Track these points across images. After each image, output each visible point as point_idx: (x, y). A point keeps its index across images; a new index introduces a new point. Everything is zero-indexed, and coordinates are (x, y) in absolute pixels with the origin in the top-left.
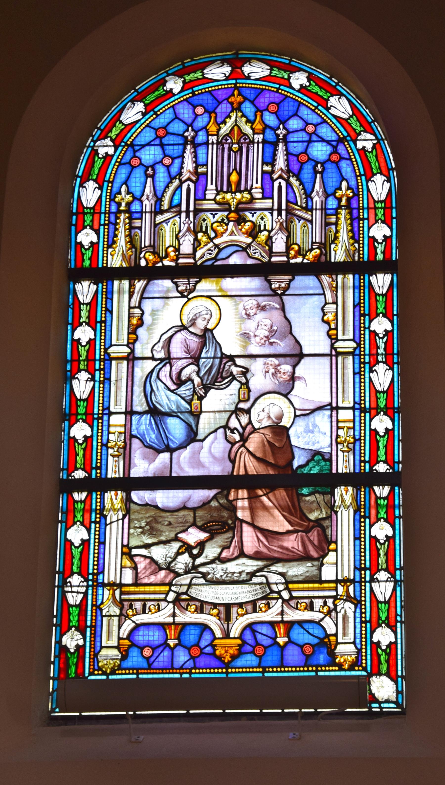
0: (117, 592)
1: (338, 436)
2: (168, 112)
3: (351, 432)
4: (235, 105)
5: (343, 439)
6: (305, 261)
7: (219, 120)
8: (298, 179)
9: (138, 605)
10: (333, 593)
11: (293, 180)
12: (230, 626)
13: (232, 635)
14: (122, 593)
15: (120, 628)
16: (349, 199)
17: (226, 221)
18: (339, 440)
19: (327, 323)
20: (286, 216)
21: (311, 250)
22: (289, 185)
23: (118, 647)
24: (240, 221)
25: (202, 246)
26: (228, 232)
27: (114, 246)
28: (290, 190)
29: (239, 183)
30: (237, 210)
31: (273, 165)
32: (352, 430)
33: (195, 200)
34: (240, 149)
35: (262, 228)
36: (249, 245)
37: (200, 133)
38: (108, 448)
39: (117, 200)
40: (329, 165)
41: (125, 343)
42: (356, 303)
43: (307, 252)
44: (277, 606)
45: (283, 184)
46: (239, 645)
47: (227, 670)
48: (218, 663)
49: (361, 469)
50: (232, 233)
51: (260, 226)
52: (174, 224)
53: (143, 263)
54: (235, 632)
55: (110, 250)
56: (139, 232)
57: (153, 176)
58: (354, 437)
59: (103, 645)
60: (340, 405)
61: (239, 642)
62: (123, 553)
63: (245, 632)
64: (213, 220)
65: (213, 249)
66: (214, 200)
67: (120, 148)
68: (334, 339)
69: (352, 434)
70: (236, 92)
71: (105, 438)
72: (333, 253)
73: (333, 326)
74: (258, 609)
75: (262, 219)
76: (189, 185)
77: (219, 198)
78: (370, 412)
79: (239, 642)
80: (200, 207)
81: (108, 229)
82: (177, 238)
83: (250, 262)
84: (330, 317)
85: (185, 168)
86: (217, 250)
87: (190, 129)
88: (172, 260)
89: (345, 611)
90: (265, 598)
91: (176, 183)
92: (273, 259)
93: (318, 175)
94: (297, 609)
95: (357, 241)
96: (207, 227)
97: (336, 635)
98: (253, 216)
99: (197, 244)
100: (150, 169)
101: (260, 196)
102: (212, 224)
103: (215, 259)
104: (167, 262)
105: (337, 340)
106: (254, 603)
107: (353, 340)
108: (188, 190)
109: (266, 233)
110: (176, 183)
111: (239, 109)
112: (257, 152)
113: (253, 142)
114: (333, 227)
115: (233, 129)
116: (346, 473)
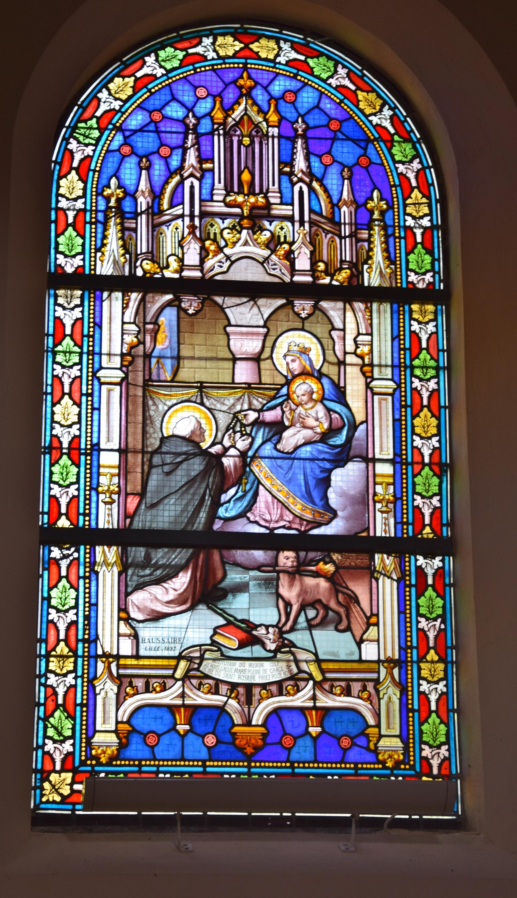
0: (114, 667)
1: (375, 494)
2: (163, 92)
5: (106, 488)
6: (334, 283)
8: (322, 185)
9: (140, 683)
10: (374, 676)
11: (315, 185)
12: (252, 710)
13: (254, 723)
14: (118, 667)
15: (117, 710)
16: (119, 201)
18: (376, 498)
20: (310, 227)
21: (341, 269)
22: (312, 190)
23: (116, 731)
24: (256, 228)
25: (210, 257)
26: (241, 242)
27: (370, 262)
28: (313, 196)
29: (252, 184)
30: (251, 217)
31: (292, 166)
32: (117, 478)
33: (201, 200)
34: (252, 142)
35: (282, 239)
37: (203, 121)
38: (98, 493)
39: (105, 193)
40: (356, 169)
41: (119, 366)
43: (335, 271)
44: (308, 690)
45: (305, 189)
46: (263, 734)
47: (249, 764)
48: (239, 755)
49: (403, 533)
50: (246, 243)
51: (279, 237)
52: (177, 229)
54: (258, 718)
55: (99, 254)
57: (148, 169)
58: (394, 496)
59: (97, 729)
60: (377, 456)
61: (263, 730)
62: (120, 619)
63: (269, 719)
64: (223, 226)
65: (224, 260)
66: (224, 201)
67: (107, 132)
68: (369, 377)
69: (117, 481)
70: (245, 75)
71: (95, 482)
72: (366, 275)
74: (285, 692)
76: (301, 188)
77: (228, 199)
78: (50, 453)
79: (263, 730)
80: (209, 209)
81: (96, 228)
83: (268, 279)
85: (296, 167)
86: (229, 263)
87: (190, 115)
88: (176, 271)
89: (390, 698)
90: (292, 678)
92: (296, 278)
93: (144, 172)
94: (331, 692)
95: (393, 262)
97: (378, 726)
98: (270, 225)
100: (144, 160)
101: (278, 201)
102: (222, 231)
104: (168, 274)
105: (373, 379)
106: (279, 684)
107: (392, 380)
108: (192, 187)
110: (177, 178)
111: (249, 95)
112: (272, 150)
113: (267, 135)
114: (366, 244)
115: (242, 118)
116: (108, 529)
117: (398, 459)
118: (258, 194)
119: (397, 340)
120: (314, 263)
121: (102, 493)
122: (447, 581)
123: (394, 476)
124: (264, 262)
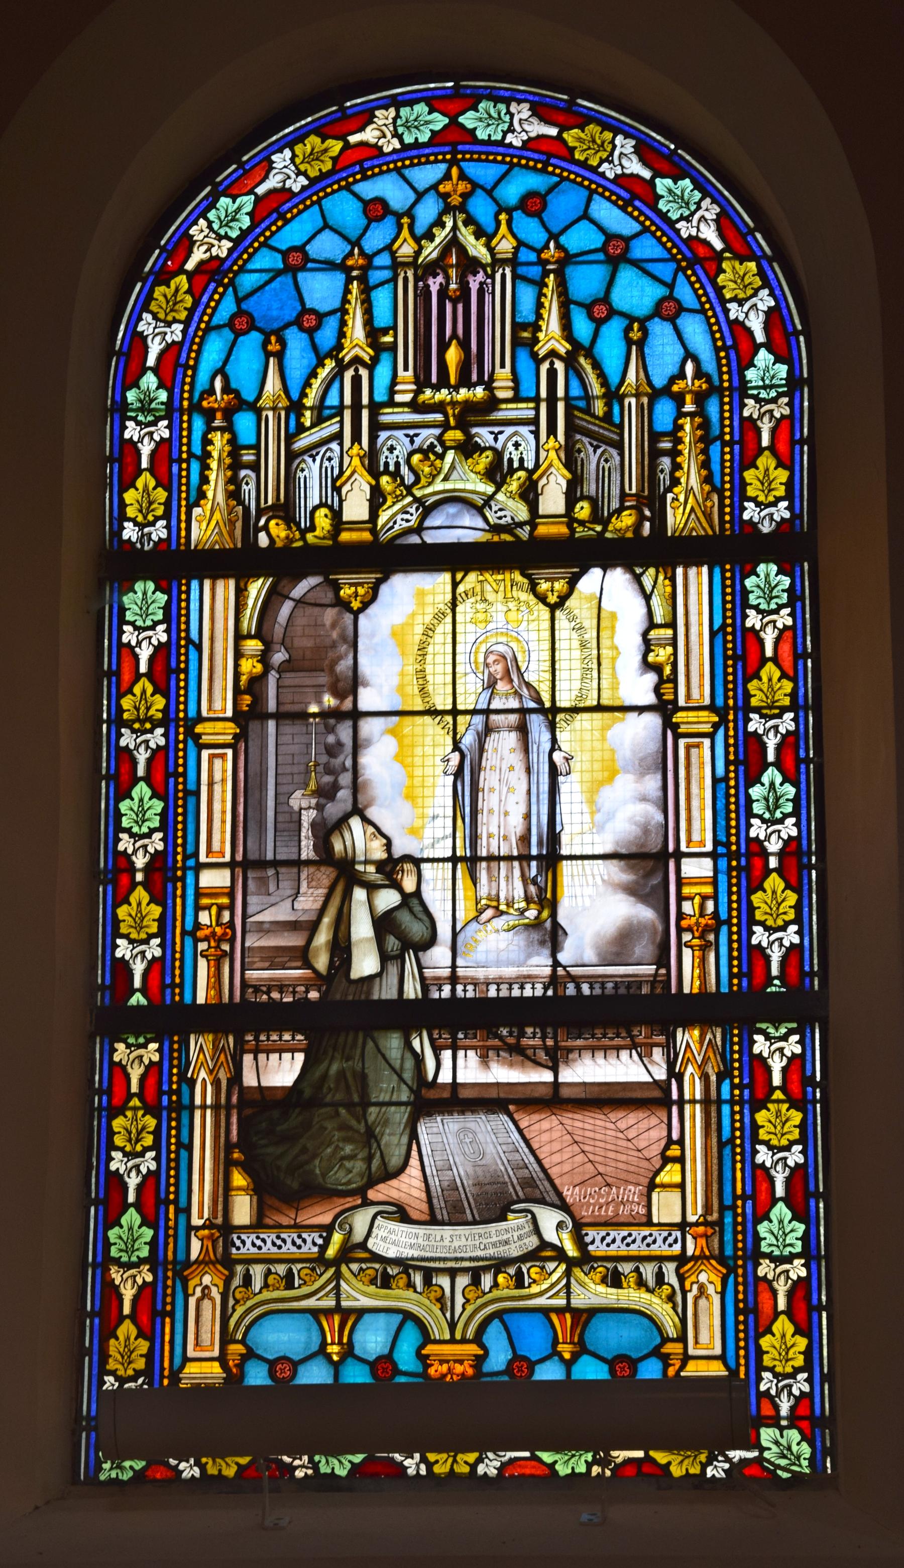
1: (680, 916)
3: (710, 906)
4: (456, 200)
7: (420, 230)
17: (439, 449)
19: (657, 668)
27: (676, 490)
35: (516, 465)
36: (489, 500)
38: (196, 941)
42: (716, 627)
43: (610, 515)
52: (330, 459)
53: (263, 540)
56: (253, 475)
57: (280, 356)
73: (667, 670)
75: (517, 445)
82: (337, 490)
84: (661, 655)
91: (330, 364)
96: (397, 464)
99: (377, 499)
103: (419, 529)
109: (522, 474)
117: (721, 850)
118: (475, 385)
119: (720, 635)
120: (571, 498)
121: (202, 940)
122: (802, 754)
123: (715, 882)
124: (484, 506)
